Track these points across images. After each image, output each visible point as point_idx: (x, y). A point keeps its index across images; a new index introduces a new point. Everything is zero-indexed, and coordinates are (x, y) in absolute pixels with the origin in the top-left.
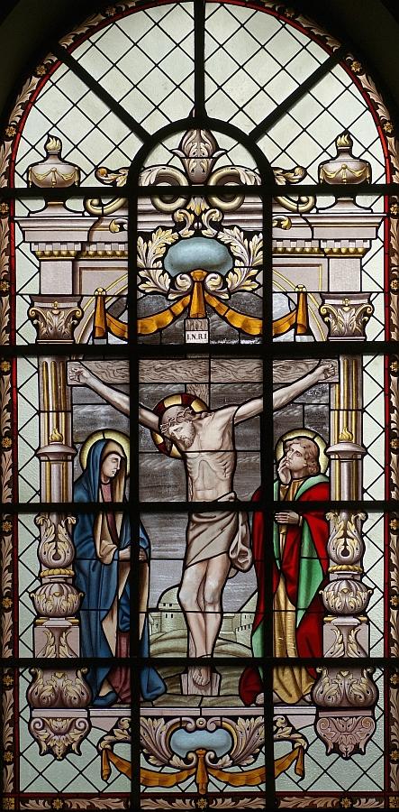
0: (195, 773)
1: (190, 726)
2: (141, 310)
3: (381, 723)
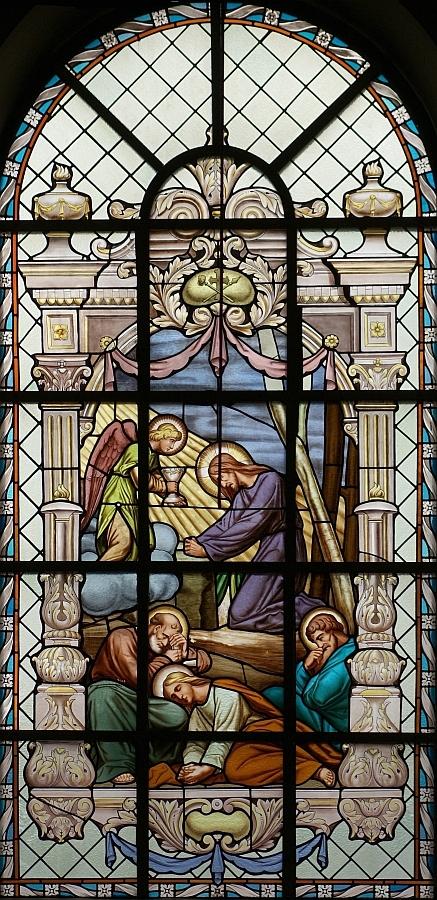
0: (212, 858)
2: (154, 353)
3: (410, 804)
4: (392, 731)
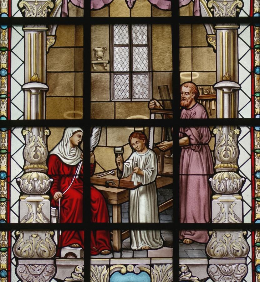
1: (124, 271)
3: (250, 266)
4: (238, 222)
